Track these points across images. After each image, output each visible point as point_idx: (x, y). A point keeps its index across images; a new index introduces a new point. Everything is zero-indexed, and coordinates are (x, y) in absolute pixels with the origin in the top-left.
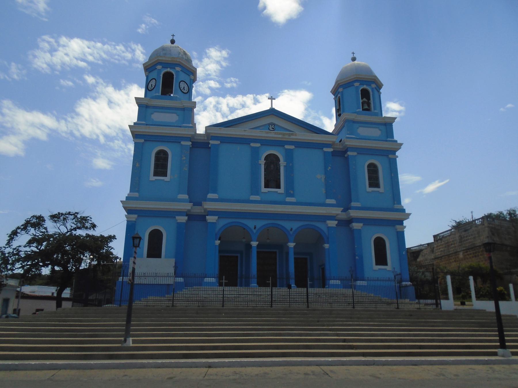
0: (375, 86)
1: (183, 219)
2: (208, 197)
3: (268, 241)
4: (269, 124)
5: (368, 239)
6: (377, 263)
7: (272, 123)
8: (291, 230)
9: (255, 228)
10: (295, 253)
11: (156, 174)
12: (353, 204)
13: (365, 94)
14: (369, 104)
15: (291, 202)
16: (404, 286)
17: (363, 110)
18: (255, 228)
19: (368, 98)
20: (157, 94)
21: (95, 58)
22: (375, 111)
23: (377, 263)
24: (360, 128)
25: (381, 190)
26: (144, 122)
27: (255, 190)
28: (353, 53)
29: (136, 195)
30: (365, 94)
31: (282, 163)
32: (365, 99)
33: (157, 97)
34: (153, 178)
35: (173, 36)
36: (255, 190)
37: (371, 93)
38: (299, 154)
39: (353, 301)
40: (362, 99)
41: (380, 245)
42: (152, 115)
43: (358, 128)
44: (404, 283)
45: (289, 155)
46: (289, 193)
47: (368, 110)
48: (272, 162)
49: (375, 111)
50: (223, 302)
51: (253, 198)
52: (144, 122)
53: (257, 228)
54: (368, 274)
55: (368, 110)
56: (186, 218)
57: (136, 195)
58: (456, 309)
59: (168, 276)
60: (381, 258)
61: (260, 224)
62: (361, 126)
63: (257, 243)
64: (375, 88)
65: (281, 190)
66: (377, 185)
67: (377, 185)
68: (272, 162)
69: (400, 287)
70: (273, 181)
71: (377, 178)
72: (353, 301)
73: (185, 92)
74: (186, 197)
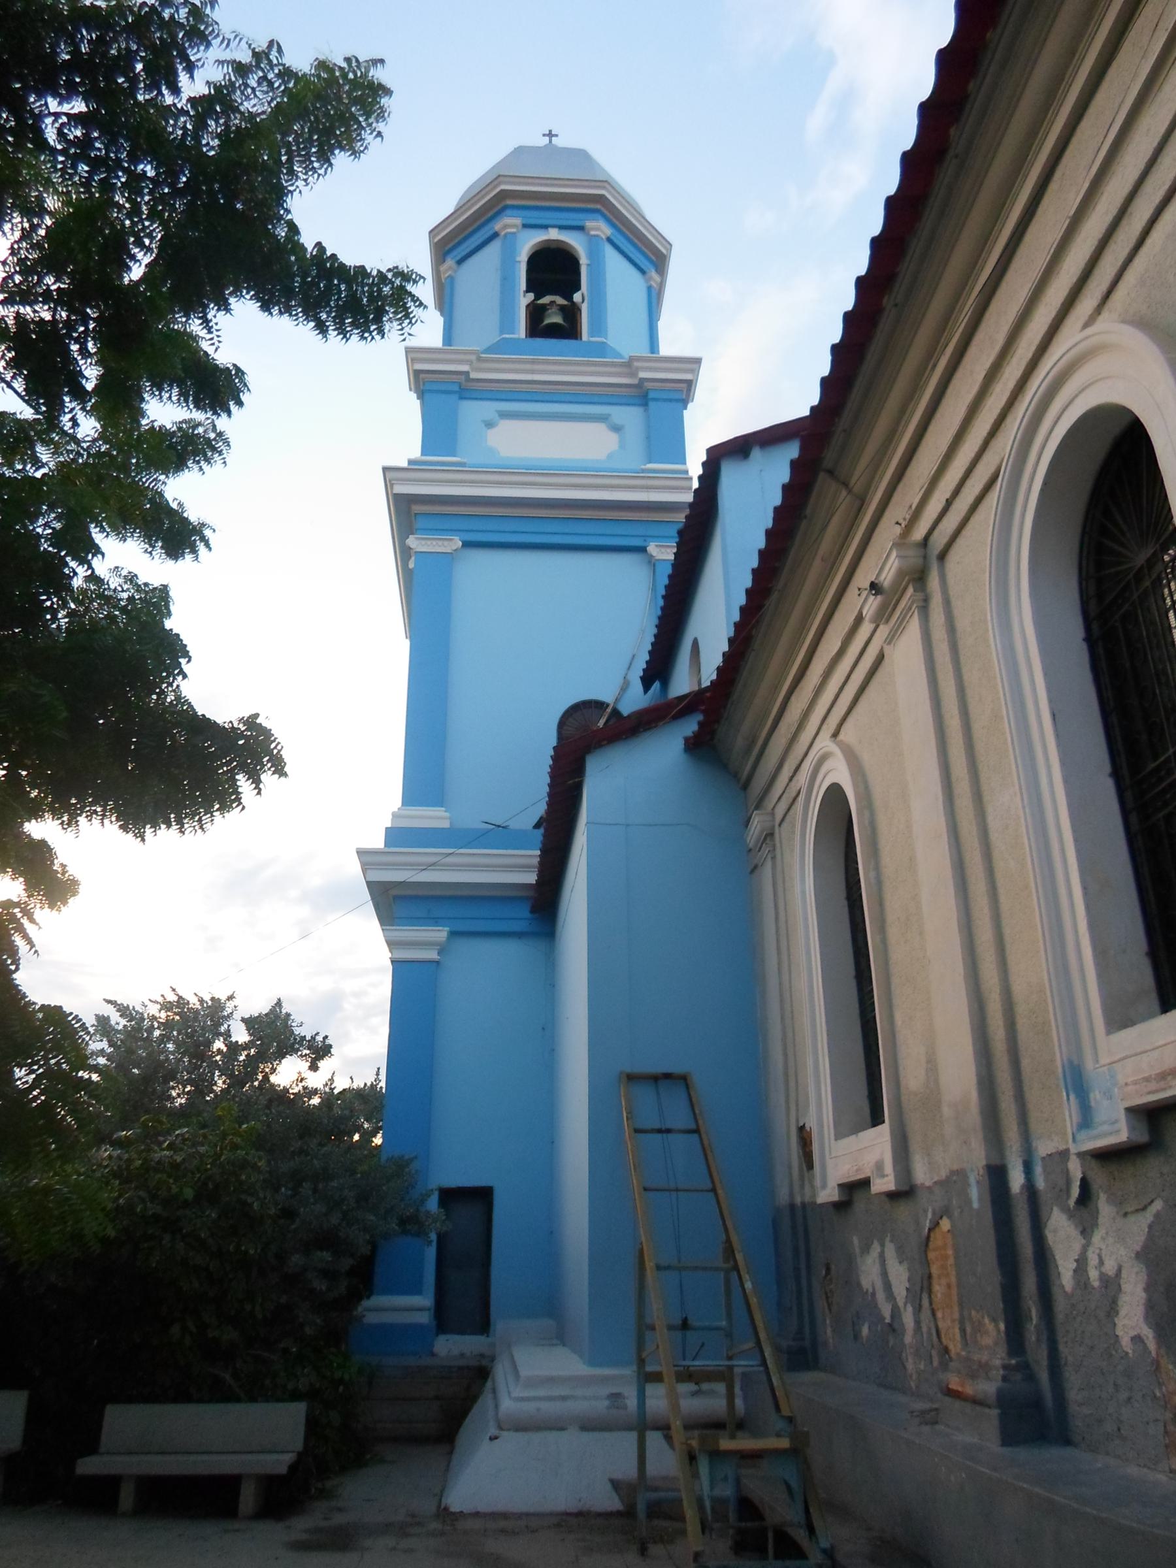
2: (297, 1411)
13: (554, 272)
28: (550, 135)
29: (435, 817)
30: (554, 272)
35: (550, 135)
43: (490, 425)
47: (569, 329)
55: (569, 329)
62: (504, 415)
64: (609, 240)
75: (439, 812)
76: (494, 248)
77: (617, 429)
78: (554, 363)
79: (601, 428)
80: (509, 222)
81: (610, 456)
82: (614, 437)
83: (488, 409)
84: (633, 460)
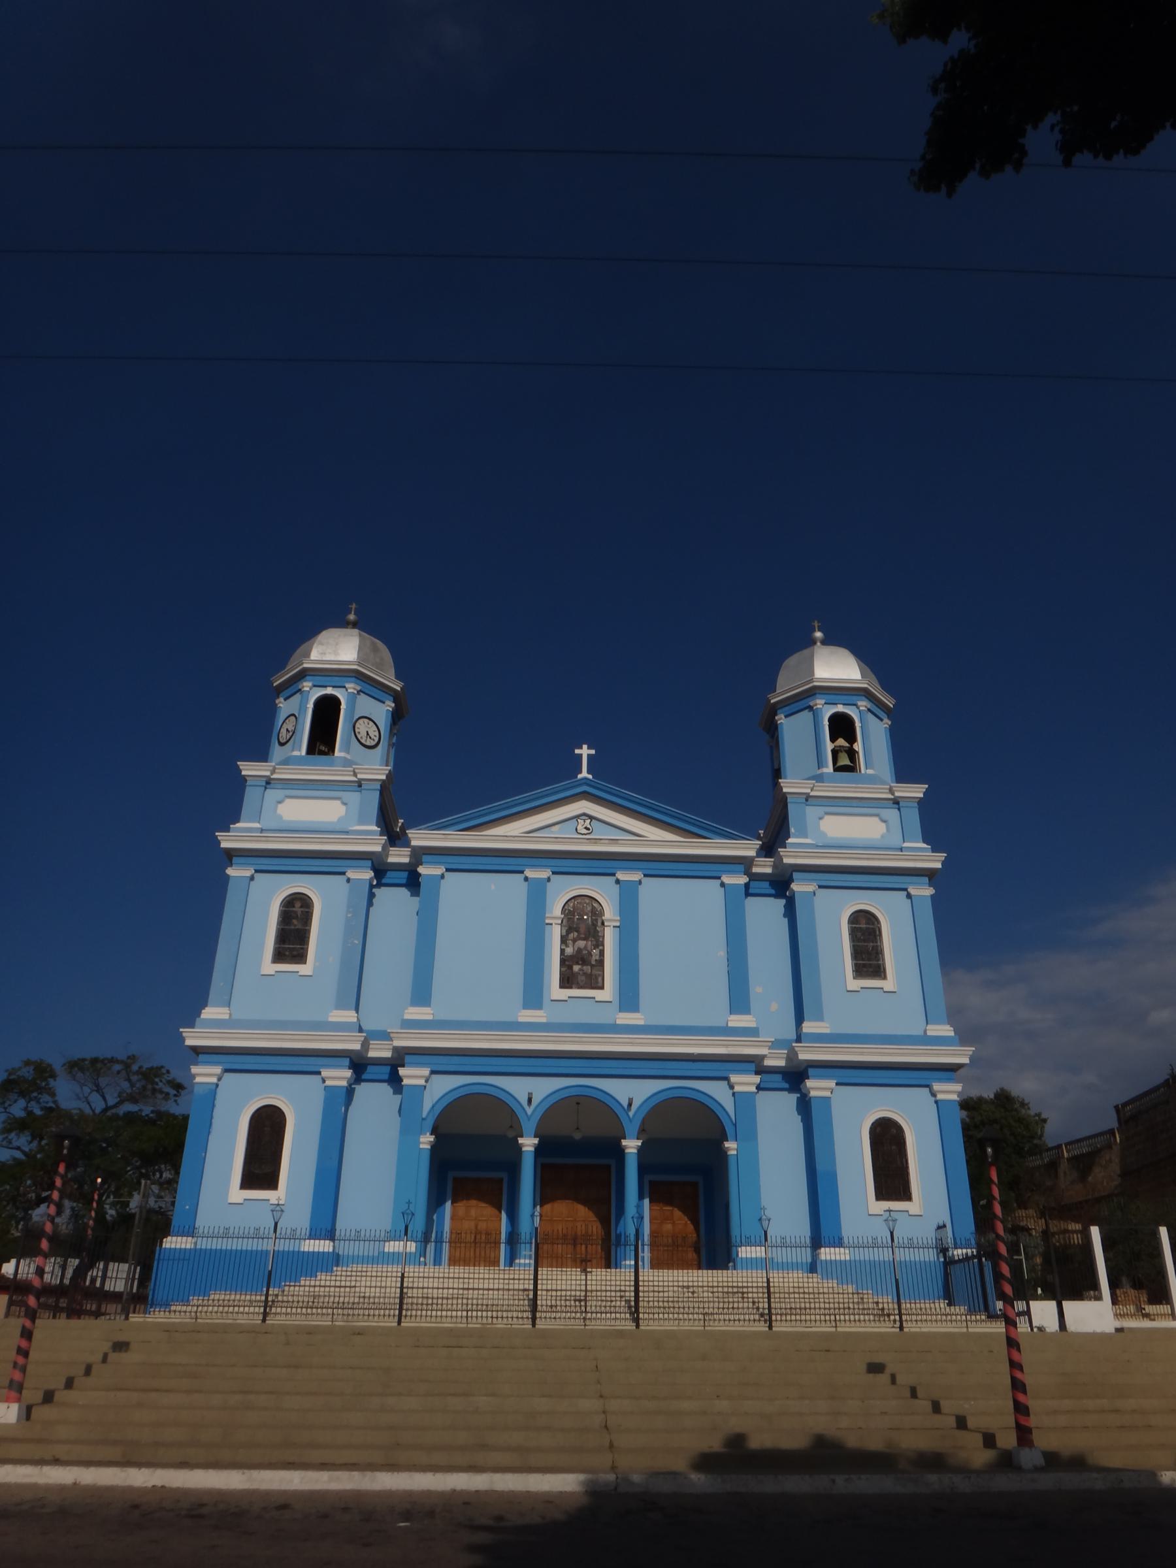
0: (869, 705)
1: (339, 1076)
3: (577, 1136)
4: (577, 817)
5: (853, 1115)
6: (881, 1195)
7: (584, 814)
8: (630, 1105)
9: (530, 1101)
10: (642, 1170)
11: (280, 956)
12: (808, 1027)
14: (852, 754)
15: (486, 1022)
16: (960, 1261)
17: (837, 769)
18: (530, 1101)
19: (852, 739)
20: (296, 753)
21: (303, 674)
22: (870, 771)
23: (881, 1195)
24: (827, 817)
25: (888, 984)
26: (257, 825)
27: (533, 996)
31: (610, 913)
32: (841, 742)
33: (298, 761)
34: (854, 984)
36: (533, 996)
37: (858, 725)
38: (656, 895)
39: (770, 1308)
40: (833, 740)
41: (887, 1141)
42: (280, 806)
43: (821, 818)
44: (959, 1253)
45: (629, 899)
46: (629, 999)
47: (851, 768)
48: (582, 922)
49: (870, 771)
50: (401, 1309)
51: (737, 1021)
52: (257, 825)
53: (535, 1102)
54: (850, 1227)
55: (851, 768)
56: (348, 1073)
58: (1119, 1330)
59: (875, 1245)
60: (892, 1180)
62: (827, 814)
63: (536, 1141)
65: (608, 993)
66: (878, 972)
67: (878, 972)
68: (582, 922)
69: (949, 1263)
70: (580, 971)
71: (878, 952)
72: (770, 1308)
73: (369, 743)
74: (947, 1031)
75: (226, 1010)
76: (297, 697)
78: (319, 771)
79: (338, 802)
80: (306, 685)
81: (882, 836)
82: (344, 808)
83: (820, 810)
84: (896, 840)
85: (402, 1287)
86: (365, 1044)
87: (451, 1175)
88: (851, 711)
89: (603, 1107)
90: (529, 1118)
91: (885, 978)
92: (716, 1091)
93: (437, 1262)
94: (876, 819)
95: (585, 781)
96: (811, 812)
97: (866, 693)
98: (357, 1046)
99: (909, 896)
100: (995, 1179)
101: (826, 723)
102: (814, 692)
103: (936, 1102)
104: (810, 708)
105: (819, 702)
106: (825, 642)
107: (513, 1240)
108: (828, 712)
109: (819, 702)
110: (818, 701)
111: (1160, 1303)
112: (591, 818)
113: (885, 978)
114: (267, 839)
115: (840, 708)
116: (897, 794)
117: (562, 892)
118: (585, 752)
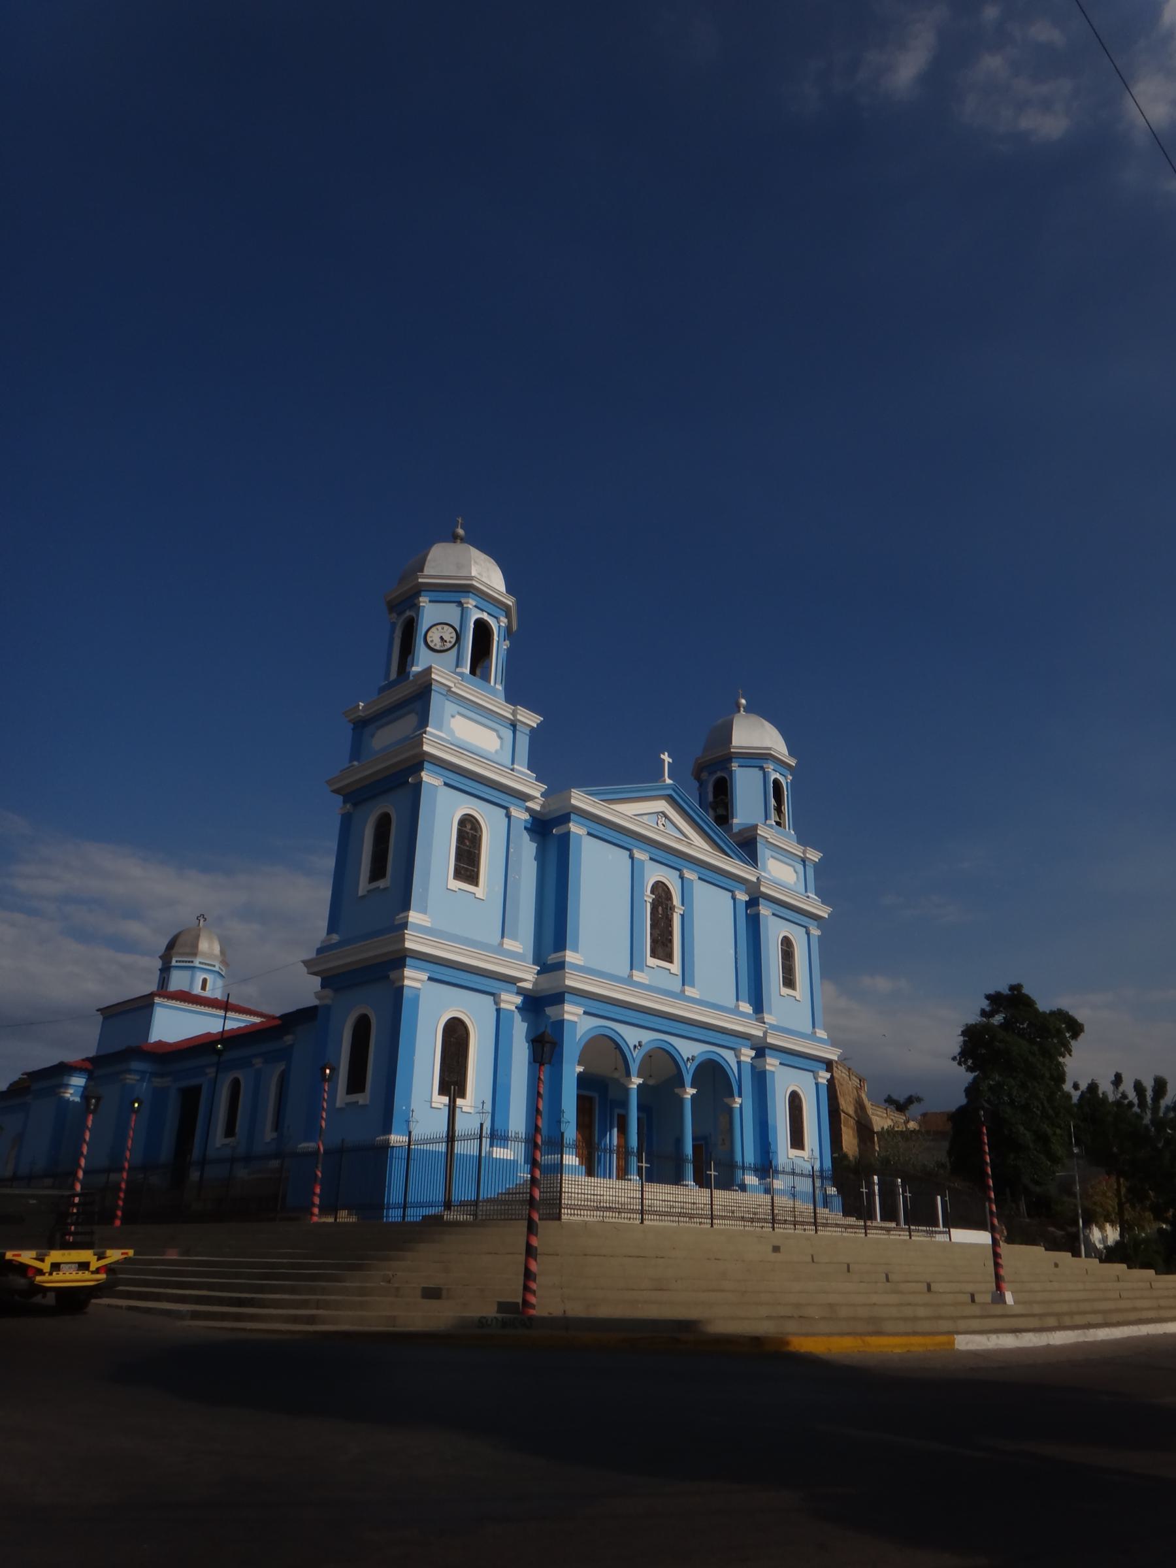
4: (657, 813)
24: (458, 717)
25: (479, 891)
43: (453, 716)
46: (686, 977)
57: (335, 938)
61: (647, 1037)
74: (822, 1034)
77: (500, 737)
81: (496, 752)
85: (642, 1199)
86: (765, 1033)
87: (595, 1095)
88: (492, 621)
89: (617, 1047)
90: (636, 1059)
91: (477, 885)
92: (729, 1055)
93: (623, 1174)
94: (791, 869)
95: (668, 787)
96: (450, 707)
97: (507, 610)
98: (761, 1034)
99: (632, 857)
100: (988, 1160)
101: (472, 626)
102: (468, 589)
103: (498, 1010)
104: (460, 604)
105: (470, 603)
106: (748, 710)
107: (624, 1152)
108: (476, 615)
109: (470, 603)
110: (471, 601)
111: (891, 1221)
112: (666, 817)
113: (477, 885)
114: (460, 755)
115: (485, 616)
116: (519, 717)
117: (655, 874)
118: (666, 757)
